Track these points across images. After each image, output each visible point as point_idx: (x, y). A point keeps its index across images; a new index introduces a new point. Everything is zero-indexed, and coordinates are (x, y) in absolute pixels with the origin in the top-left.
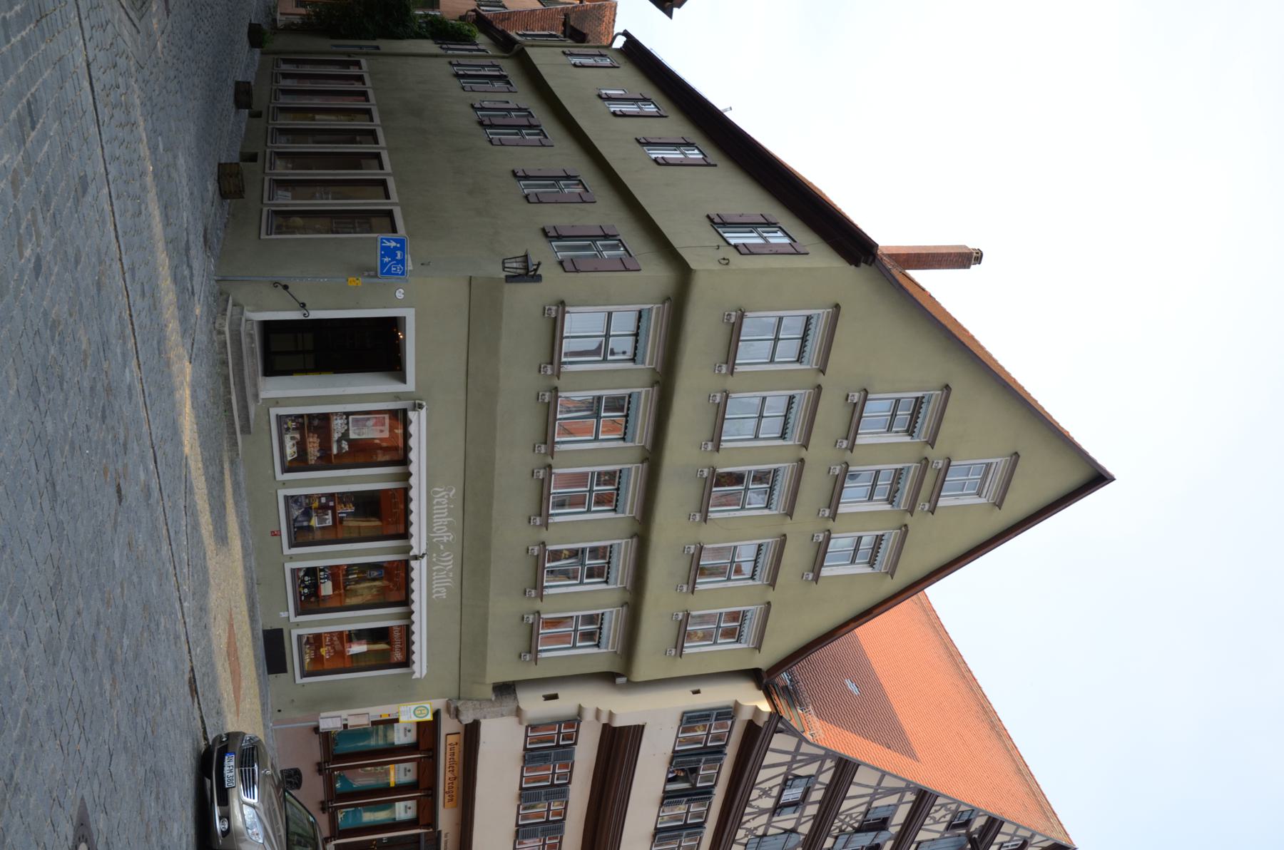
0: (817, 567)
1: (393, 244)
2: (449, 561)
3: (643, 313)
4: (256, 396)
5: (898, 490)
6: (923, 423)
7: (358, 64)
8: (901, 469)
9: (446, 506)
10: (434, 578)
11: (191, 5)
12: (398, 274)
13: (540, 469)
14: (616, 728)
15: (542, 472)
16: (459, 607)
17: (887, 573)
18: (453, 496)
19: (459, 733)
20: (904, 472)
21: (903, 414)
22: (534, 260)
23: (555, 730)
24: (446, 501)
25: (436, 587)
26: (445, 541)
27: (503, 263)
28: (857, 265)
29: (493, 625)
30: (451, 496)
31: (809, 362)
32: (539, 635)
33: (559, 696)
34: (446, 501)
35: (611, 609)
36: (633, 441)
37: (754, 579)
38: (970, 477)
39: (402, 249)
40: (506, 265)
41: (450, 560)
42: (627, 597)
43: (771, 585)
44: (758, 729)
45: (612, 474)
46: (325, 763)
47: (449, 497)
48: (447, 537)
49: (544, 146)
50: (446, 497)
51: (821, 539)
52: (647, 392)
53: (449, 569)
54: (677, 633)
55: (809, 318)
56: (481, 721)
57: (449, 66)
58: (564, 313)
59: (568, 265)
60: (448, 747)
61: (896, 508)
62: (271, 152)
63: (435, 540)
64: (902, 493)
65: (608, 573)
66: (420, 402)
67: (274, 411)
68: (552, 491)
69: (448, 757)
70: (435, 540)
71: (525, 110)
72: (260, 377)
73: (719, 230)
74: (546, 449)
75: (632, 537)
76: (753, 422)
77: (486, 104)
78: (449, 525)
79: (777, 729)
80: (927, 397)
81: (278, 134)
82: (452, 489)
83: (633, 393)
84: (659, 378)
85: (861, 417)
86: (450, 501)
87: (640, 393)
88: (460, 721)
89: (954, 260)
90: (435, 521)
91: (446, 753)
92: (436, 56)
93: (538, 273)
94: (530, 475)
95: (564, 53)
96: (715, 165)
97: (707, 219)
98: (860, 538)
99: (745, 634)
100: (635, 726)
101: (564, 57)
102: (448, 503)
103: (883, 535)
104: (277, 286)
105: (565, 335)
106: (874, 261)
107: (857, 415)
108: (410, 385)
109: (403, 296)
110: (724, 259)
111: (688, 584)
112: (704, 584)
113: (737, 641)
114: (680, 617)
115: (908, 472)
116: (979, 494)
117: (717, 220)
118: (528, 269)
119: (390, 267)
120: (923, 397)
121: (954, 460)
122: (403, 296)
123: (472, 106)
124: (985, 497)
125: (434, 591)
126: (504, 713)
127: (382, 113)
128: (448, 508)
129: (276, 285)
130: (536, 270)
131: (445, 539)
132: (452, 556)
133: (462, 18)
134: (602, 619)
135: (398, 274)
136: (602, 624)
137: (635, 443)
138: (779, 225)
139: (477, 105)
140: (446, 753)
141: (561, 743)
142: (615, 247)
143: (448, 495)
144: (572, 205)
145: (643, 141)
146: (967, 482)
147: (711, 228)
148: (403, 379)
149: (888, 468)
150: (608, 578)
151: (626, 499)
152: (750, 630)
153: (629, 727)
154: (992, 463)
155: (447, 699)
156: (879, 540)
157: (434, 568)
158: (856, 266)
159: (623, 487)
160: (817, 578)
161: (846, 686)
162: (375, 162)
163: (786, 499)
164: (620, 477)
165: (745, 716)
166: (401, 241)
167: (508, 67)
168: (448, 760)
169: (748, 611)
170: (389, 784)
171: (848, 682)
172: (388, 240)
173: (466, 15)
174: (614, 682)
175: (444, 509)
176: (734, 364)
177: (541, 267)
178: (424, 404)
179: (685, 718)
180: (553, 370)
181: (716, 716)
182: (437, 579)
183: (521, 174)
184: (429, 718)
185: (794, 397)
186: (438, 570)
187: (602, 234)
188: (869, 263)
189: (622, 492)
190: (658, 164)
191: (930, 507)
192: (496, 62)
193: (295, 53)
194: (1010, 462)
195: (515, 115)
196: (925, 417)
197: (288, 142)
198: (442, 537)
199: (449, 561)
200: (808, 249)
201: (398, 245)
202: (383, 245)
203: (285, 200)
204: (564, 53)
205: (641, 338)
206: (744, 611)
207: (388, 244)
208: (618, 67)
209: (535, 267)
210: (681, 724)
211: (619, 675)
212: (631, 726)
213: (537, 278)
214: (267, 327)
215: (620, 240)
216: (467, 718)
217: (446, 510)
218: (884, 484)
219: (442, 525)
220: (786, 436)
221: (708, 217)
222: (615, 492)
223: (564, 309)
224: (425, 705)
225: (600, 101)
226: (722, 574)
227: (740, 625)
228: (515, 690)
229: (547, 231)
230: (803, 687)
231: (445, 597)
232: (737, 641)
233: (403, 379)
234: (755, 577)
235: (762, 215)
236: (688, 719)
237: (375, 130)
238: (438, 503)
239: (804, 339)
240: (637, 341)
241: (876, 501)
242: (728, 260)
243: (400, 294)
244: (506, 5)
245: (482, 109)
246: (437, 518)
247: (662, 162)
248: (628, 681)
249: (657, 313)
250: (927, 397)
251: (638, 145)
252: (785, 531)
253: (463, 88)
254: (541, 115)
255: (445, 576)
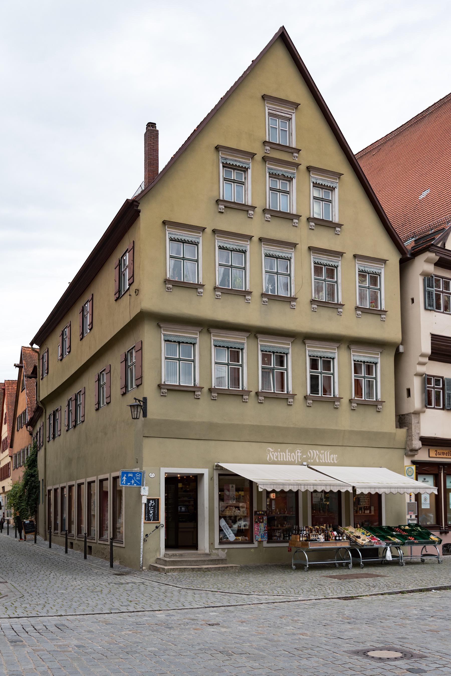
0: (332, 226)
1: (124, 478)
2: (313, 452)
3: (166, 339)
4: (207, 554)
5: (283, 175)
6: (240, 162)
7: (49, 491)
8: (269, 174)
9: (279, 453)
10: (324, 462)
11: (8, 572)
12: (141, 476)
13: (258, 399)
14: (432, 352)
15: (260, 398)
16: (344, 447)
17: (339, 178)
18: (273, 449)
19: (429, 450)
20: (272, 171)
21: (234, 175)
22: (133, 402)
23: (432, 390)
24: (276, 453)
25: (330, 460)
26: (301, 454)
27: (134, 418)
28: (139, 211)
29: (357, 427)
30: (273, 450)
31: (198, 238)
32: (365, 400)
33: (408, 387)
34: (276, 453)
35: (352, 356)
36: (243, 344)
37: (245, 251)
38: (277, 127)
39: (127, 473)
40: (136, 417)
41: (313, 452)
42: (344, 347)
43: (342, 255)
44: (441, 260)
45: (264, 356)
46: (440, 530)
47: (273, 451)
48: (298, 454)
49: (85, 392)
50: (273, 453)
51: (313, 224)
52: (214, 336)
53: (319, 453)
54: (371, 315)
55: (171, 240)
56: (420, 436)
57: (50, 442)
58: (165, 385)
59: (139, 382)
60: (438, 456)
61: (296, 175)
62: (99, 540)
63: (300, 460)
64: (286, 172)
65: (327, 358)
66: (215, 466)
67: (217, 545)
68: (272, 391)
69: (445, 456)
70: (300, 460)
71: (69, 402)
72: (198, 552)
73: (122, 294)
74: (246, 395)
75: (257, 338)
76: (234, 270)
77: (66, 424)
78: (291, 452)
79: (442, 247)
80: (223, 161)
81: (90, 536)
82: (269, 449)
83: (164, 339)
84: (205, 330)
85: (234, 203)
86: (276, 451)
87: (214, 340)
88: (420, 449)
89: (153, 141)
90: (287, 460)
91: (442, 458)
92: (45, 449)
93: (142, 399)
94: (262, 405)
95: (42, 379)
96: (93, 295)
97: (117, 301)
98: (315, 198)
99: (374, 270)
100: (432, 340)
101: (44, 379)
102: (277, 453)
103: (313, 182)
104: (146, 540)
105: (178, 384)
106: (136, 201)
107: (232, 206)
108: (205, 472)
109: (153, 474)
110: (136, 292)
111: (337, 308)
112: (340, 298)
113: (379, 275)
114: (316, 306)
115: (271, 169)
116: (290, 119)
117: (117, 295)
118: (138, 405)
119: (137, 480)
120: (223, 163)
121: (266, 139)
122: (153, 474)
123: (67, 431)
124: (292, 115)
125: (332, 462)
126: (416, 422)
127: (70, 480)
128: (280, 453)
129: (145, 541)
130: (139, 401)
131: (299, 454)
132: (311, 451)
133: (31, 434)
134: (358, 361)
135: (141, 476)
136: (361, 361)
137: (245, 343)
138: (120, 259)
139: (67, 428)
140: (442, 458)
141: (441, 386)
142: (131, 354)
143: (272, 452)
144: (111, 378)
145: (81, 337)
146: (280, 128)
147: (121, 299)
148: (202, 475)
149: (269, 182)
150: (331, 358)
151: (280, 347)
152: (371, 268)
153: (432, 344)
154: (268, 113)
155: (405, 456)
156: (316, 185)
157: (318, 461)
158: (140, 212)
159: (272, 350)
160: (340, 225)
161: (423, 199)
162: (104, 482)
163: (284, 248)
164: (266, 351)
165: (430, 268)
166: (123, 473)
167: (50, 411)
168: (447, 456)
169: (359, 269)
170: (436, 495)
171: (421, 197)
172: (122, 480)
173: (29, 431)
174: (403, 353)
175: (280, 455)
176: (198, 284)
177: (136, 398)
178: (216, 464)
179: (429, 308)
180: (198, 391)
181: (430, 287)
182: (325, 460)
183: (97, 406)
184: (414, 467)
185: (220, 246)
186: (319, 458)
187: (124, 362)
188: (138, 204)
189: (275, 350)
190: (92, 328)
191: (296, 153)
192: (48, 417)
193: (45, 523)
194: (267, 100)
195: (72, 407)
196: (236, 161)
197: (107, 530)
198: (298, 456)
199: (313, 452)
200: (132, 241)
201: (125, 475)
202: (124, 483)
203: (109, 534)
204: (42, 379)
205: (181, 340)
206: (359, 272)
207: (124, 480)
208: (48, 349)
209: (137, 401)
210: (433, 310)
211: (398, 349)
212: (431, 342)
213: (145, 399)
214: (168, 547)
215: (128, 352)
216: (417, 444)
217: (281, 453)
218: (279, 185)
219: (290, 456)
220: (244, 250)
221: (116, 300)
222: (275, 354)
223: (163, 385)
224: (406, 469)
225: (63, 360)
226: (333, 286)
227: (369, 273)
228: (403, 415)
229: (123, 393)
230: (434, 222)
231: (337, 456)
232: (379, 275)
233: (202, 475)
234: (336, 266)
235: (115, 269)
236: (430, 306)
237: (78, 484)
238: (277, 458)
239: (184, 242)
240: (183, 342)
241: (290, 189)
242: (136, 290)
243: (153, 475)
244: (25, 409)
245: (68, 426)
246: (286, 459)
247: (91, 326)
248: (402, 344)
249: (167, 331)
250: (223, 161)
251: (83, 339)
252: (306, 248)
253: (59, 435)
254: (71, 394)
255: (323, 455)
